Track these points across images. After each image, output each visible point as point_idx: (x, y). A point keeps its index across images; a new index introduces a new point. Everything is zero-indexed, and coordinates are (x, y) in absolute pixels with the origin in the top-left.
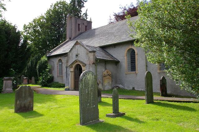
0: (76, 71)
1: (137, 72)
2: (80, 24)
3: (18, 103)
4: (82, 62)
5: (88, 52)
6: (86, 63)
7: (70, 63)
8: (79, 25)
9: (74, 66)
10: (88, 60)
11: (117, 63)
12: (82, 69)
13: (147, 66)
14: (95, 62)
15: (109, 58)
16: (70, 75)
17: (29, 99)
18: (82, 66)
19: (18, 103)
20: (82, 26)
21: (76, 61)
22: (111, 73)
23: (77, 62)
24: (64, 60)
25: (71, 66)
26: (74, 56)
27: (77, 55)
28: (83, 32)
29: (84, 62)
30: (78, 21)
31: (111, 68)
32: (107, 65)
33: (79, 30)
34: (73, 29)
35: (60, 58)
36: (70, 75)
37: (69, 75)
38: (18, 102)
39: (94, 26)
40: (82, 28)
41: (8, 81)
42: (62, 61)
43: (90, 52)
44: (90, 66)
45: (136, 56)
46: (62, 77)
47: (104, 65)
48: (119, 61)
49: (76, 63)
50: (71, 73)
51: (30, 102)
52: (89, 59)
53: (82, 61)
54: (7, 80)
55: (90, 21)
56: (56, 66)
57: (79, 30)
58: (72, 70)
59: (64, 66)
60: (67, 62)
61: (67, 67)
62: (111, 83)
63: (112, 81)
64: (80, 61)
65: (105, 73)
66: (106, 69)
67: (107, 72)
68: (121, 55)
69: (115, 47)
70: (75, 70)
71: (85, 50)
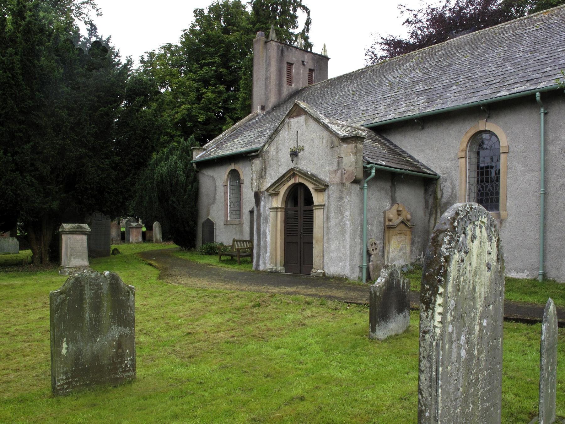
0: (289, 206)
1: (503, 213)
2: (292, 64)
3: (64, 351)
4: (312, 178)
5: (336, 142)
6: (327, 179)
7: (268, 183)
8: (290, 65)
9: (283, 190)
10: (335, 167)
11: (427, 182)
12: (313, 203)
13: (545, 194)
14: (360, 175)
15: (395, 166)
16: (271, 221)
17: (116, 332)
18: (312, 191)
19: (64, 351)
20: (298, 69)
21: (292, 173)
22: (409, 217)
23: (294, 175)
24: (248, 173)
25: (273, 191)
26: (285, 156)
27: (294, 154)
28: (300, 87)
29: (322, 176)
30: (286, 53)
31: (410, 199)
32: (397, 189)
33: (290, 82)
34: (273, 77)
35: (232, 167)
36: (271, 221)
37: (266, 219)
38: (65, 345)
39: (334, 71)
40: (300, 78)
41: (75, 236)
42: (241, 174)
43: (344, 140)
44: (341, 192)
45: (503, 157)
46: (240, 224)
47: (389, 188)
48: (436, 175)
49: (292, 182)
50: (272, 214)
51: (119, 345)
52: (338, 166)
53: (315, 172)
54: (71, 232)
55: (321, 56)
56: (220, 190)
57: (290, 82)
58: (277, 202)
59: (248, 195)
60: (262, 176)
61: (257, 197)
62: (408, 248)
63: (412, 243)
64: (305, 175)
65: (391, 216)
66: (394, 201)
67: (399, 213)
68: (444, 155)
69: (423, 128)
70: (286, 204)
71: (326, 133)
